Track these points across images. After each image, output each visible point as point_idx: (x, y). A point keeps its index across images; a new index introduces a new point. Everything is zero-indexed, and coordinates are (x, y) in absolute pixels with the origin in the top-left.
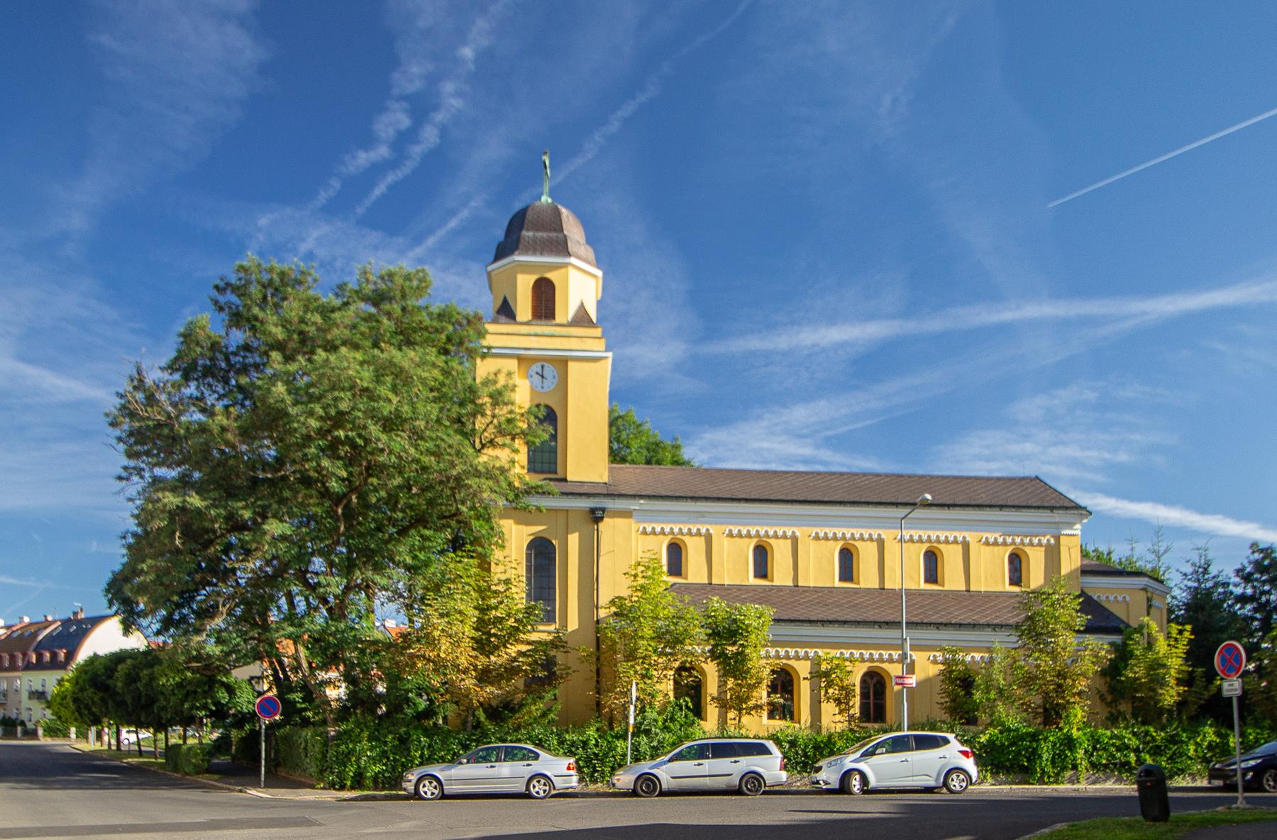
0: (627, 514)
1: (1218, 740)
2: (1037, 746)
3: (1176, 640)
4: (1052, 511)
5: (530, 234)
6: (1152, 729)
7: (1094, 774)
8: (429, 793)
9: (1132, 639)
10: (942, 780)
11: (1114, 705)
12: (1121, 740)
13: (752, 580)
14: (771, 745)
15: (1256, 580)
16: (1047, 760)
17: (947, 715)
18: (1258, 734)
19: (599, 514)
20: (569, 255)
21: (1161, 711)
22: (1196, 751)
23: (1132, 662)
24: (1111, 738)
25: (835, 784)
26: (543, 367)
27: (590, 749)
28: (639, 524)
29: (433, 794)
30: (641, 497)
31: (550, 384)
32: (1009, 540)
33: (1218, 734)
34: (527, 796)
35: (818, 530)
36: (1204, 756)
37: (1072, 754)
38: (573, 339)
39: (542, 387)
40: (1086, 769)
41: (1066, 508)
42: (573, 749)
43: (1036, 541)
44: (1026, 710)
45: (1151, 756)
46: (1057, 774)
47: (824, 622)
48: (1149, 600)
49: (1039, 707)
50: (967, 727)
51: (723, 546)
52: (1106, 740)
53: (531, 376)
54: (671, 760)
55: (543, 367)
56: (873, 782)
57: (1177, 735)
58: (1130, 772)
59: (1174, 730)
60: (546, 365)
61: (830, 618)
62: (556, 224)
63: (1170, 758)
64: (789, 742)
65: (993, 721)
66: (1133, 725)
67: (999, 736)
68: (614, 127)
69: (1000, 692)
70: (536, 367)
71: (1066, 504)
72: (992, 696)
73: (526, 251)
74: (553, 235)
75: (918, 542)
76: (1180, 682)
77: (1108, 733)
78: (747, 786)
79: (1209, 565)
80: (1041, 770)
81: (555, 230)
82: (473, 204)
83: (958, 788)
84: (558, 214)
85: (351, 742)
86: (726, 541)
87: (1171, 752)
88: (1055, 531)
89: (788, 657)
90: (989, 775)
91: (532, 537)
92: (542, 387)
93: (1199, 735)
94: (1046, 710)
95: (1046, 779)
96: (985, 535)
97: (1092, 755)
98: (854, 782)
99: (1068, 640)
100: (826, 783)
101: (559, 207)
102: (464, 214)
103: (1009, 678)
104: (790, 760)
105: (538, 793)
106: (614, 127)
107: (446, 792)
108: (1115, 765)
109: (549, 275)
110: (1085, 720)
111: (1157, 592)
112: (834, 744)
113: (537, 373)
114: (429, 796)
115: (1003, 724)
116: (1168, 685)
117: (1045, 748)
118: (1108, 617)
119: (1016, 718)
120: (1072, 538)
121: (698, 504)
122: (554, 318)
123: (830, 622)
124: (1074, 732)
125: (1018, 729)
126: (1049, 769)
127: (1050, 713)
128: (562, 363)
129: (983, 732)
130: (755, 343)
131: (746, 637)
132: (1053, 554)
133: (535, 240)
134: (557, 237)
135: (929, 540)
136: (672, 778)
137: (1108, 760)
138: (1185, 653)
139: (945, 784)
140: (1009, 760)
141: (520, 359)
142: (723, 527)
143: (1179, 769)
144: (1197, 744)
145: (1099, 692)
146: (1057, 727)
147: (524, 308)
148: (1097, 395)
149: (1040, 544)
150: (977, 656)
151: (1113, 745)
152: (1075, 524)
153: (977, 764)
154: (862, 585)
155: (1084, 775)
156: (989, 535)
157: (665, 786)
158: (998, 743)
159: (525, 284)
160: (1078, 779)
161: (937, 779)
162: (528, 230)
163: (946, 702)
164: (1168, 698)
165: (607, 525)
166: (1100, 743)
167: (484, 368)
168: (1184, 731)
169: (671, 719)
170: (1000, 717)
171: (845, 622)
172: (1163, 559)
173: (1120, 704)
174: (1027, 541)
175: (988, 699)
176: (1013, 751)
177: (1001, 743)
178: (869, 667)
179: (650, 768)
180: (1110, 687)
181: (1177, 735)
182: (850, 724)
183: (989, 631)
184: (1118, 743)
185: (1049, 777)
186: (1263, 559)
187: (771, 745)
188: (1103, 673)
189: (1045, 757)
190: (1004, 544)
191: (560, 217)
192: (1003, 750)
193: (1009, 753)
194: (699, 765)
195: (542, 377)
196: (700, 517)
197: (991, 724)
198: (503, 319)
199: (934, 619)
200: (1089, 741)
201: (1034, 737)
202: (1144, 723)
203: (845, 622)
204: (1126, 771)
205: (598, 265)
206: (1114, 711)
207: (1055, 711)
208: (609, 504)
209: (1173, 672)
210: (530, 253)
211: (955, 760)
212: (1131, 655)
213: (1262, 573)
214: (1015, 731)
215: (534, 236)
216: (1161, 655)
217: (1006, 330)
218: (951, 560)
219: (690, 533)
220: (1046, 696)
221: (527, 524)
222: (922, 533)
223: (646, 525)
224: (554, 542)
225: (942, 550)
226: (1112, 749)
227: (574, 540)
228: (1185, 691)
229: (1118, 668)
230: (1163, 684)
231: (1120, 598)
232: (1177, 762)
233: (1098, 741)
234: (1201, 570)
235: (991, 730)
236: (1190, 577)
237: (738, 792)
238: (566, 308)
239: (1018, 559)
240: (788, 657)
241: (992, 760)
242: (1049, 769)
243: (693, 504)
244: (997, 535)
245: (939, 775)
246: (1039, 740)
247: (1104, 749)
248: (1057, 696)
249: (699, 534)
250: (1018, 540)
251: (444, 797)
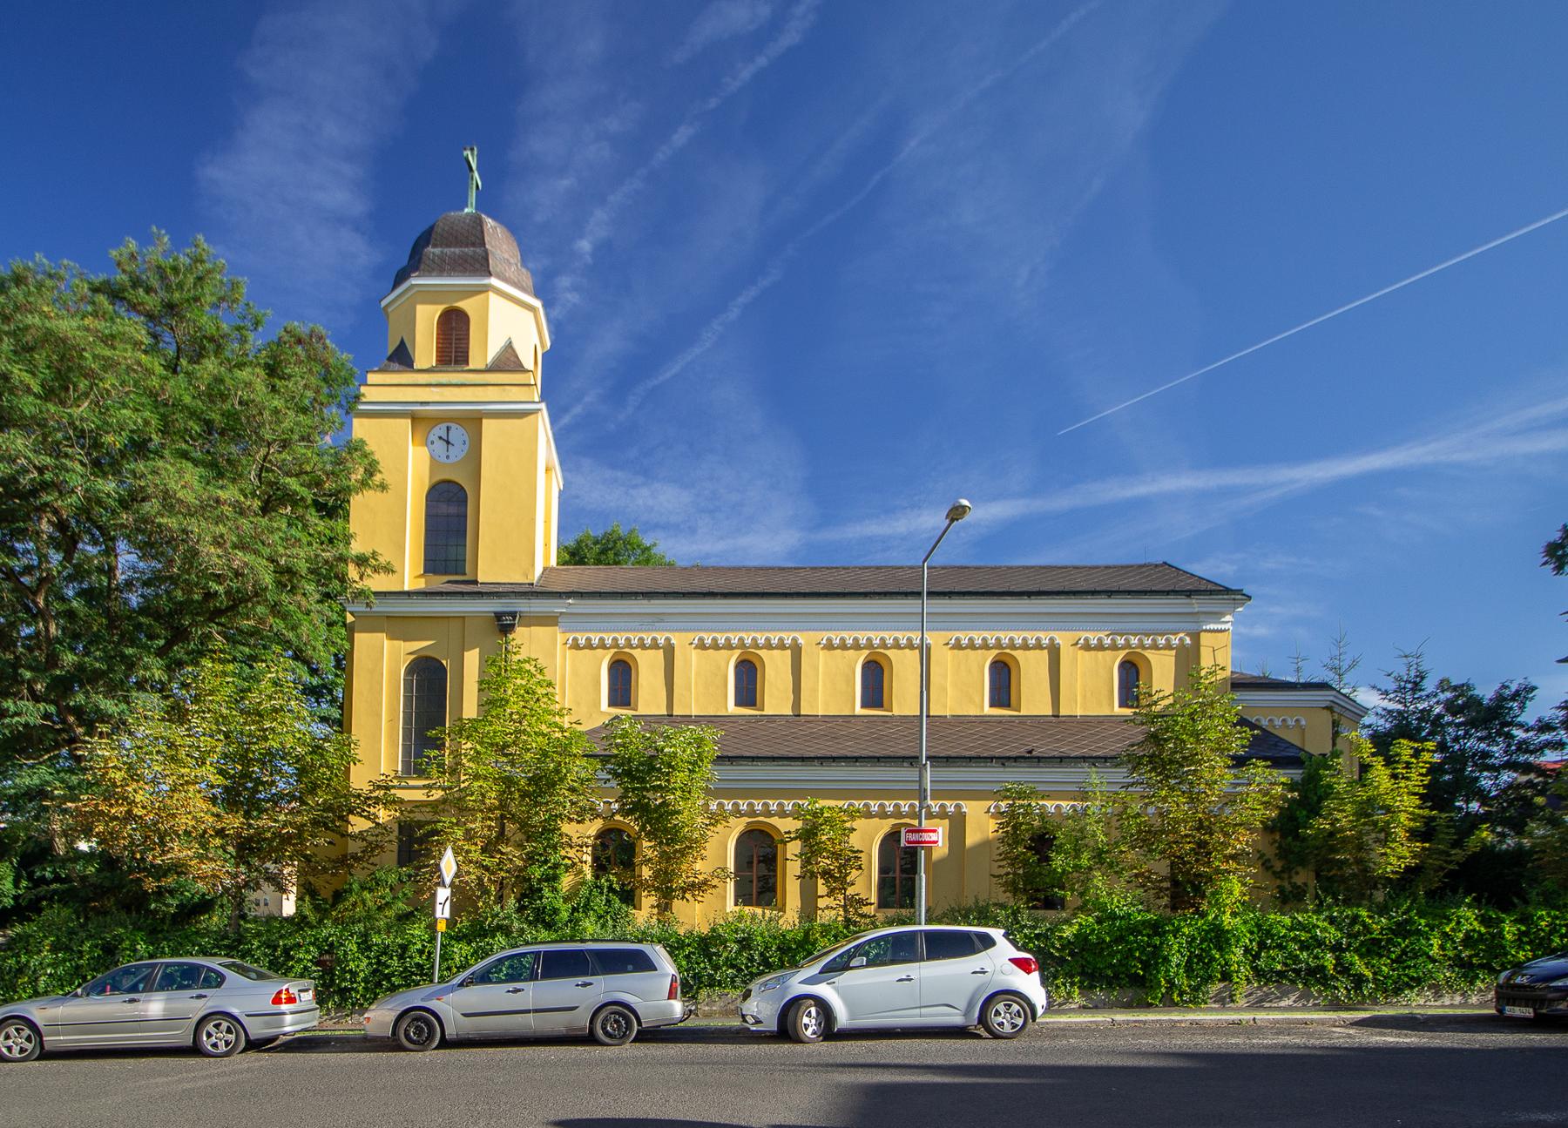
0: (549, 620)
1: (1483, 930)
2: (1161, 943)
3: (1408, 765)
4: (1189, 596)
5: (437, 251)
6: (1364, 913)
7: (1260, 988)
8: (16, 1049)
9: (1329, 768)
10: (976, 1014)
11: (1286, 876)
12: (1309, 932)
13: (732, 709)
14: (659, 954)
15: (1449, 724)
16: (1178, 965)
17: (1008, 894)
18: (1557, 918)
19: (507, 620)
20: (490, 274)
21: (1373, 883)
22: (1442, 947)
23: (1330, 803)
24: (1291, 929)
25: (772, 1025)
26: (448, 429)
27: (411, 957)
28: (568, 635)
29: (22, 1050)
30: (569, 594)
31: (458, 452)
32: (1121, 641)
33: (1484, 920)
34: (195, 1050)
35: (832, 635)
36: (1458, 956)
37: (1222, 956)
38: (490, 388)
39: (448, 457)
40: (1247, 979)
41: (1211, 592)
42: (384, 959)
43: (1161, 641)
44: (1142, 886)
45: (1361, 957)
46: (1196, 989)
47: (823, 760)
48: (1335, 724)
49: (1164, 879)
50: (1041, 913)
51: (691, 662)
52: (1284, 931)
53: (432, 443)
54: (461, 985)
55: (448, 429)
56: (843, 1019)
57: (1409, 921)
58: (1323, 985)
59: (1404, 914)
60: (453, 426)
61: (834, 755)
62: (474, 236)
63: (1398, 960)
64: (737, 941)
65: (1085, 903)
66: (1329, 907)
67: (1096, 927)
68: (734, 313)
69: (1099, 855)
70: (440, 430)
71: (1210, 587)
72: (1085, 861)
73: (429, 272)
74: (469, 250)
75: (981, 648)
76: (1414, 835)
77: (1287, 920)
78: (604, 1029)
79: (1423, 678)
80: (1168, 982)
81: (473, 245)
82: (587, 399)
83: (1007, 1029)
84: (479, 223)
85: (27, 952)
86: (695, 654)
87: (1398, 950)
88: (1192, 627)
89: (769, 814)
90: (1077, 991)
91: (413, 657)
92: (448, 457)
93: (1450, 921)
94: (1175, 883)
95: (1176, 998)
96: (1084, 635)
97: (1257, 957)
98: (806, 1020)
99: (1217, 774)
100: (758, 1022)
101: (483, 216)
102: (578, 410)
103: (1116, 834)
104: (739, 970)
105: (215, 1045)
106: (734, 313)
107: (47, 1047)
108: (1297, 972)
109: (462, 305)
110: (1246, 898)
111: (1347, 714)
112: (814, 944)
113: (440, 438)
114: (16, 1053)
115: (1103, 908)
116: (1394, 841)
117: (1176, 947)
118: (1276, 745)
119: (1125, 898)
120: (1220, 634)
121: (652, 602)
122: (468, 364)
123: (834, 759)
124: (1227, 919)
125: (1130, 915)
126: (1182, 981)
127: (1185, 889)
128: (473, 421)
129: (1067, 922)
130: (873, 528)
131: (668, 774)
132: (1188, 659)
133: (442, 258)
134: (475, 252)
135: (998, 645)
136: (465, 1015)
137: (1285, 964)
138: (1424, 786)
139: (983, 1020)
140: (1111, 966)
141: (415, 418)
142: (691, 636)
143: (1412, 979)
144: (1445, 935)
145: (1262, 856)
146: (1197, 912)
147: (425, 350)
148: (1235, 567)
149: (1168, 647)
150: (1065, 805)
151: (1295, 939)
152: (1224, 615)
153: (1044, 982)
154: (896, 712)
155: (1242, 989)
156: (1090, 635)
157: (451, 1032)
158: (1093, 938)
159: (427, 318)
160: (1231, 996)
161: (967, 1013)
162: (435, 246)
163: (1008, 874)
164: (1393, 860)
165: (520, 634)
166: (1271, 937)
167: (361, 428)
168: (1421, 914)
169: (586, 906)
170: (1098, 897)
171: (857, 759)
172: (1346, 678)
173: (1297, 873)
174: (1148, 641)
175: (1077, 868)
176: (1119, 951)
177: (1098, 938)
178: (894, 825)
179: (422, 1000)
180: (1280, 847)
181: (1409, 921)
182: (846, 911)
183: (1086, 767)
184: (1304, 936)
185: (1181, 994)
186: (1457, 697)
187: (659, 954)
188: (1269, 828)
189: (1175, 960)
190: (1114, 647)
191: (482, 227)
192: (1102, 949)
193: (1112, 955)
194: (516, 991)
195: (448, 442)
196: (658, 620)
197: (1082, 908)
198: (396, 366)
199: (998, 752)
200: (1252, 933)
201: (1156, 928)
202: (1347, 903)
203: (857, 759)
204: (1318, 981)
205: (537, 295)
206: (1286, 884)
207: (1193, 885)
208: (521, 606)
209: (1403, 817)
210: (435, 274)
211: (1004, 977)
212: (1328, 792)
213: (1454, 714)
214: (1122, 918)
215: (442, 252)
216: (1382, 790)
217: (1140, 506)
218: (1032, 671)
219: (642, 646)
220: (1177, 863)
221: (407, 638)
222: (987, 634)
223: (578, 635)
224: (444, 662)
225: (1019, 659)
226: (1293, 946)
227: (472, 659)
228: (1423, 849)
229: (1296, 819)
230: (1385, 835)
231: (1291, 722)
232: (1409, 967)
233: (1268, 934)
234: (1409, 686)
235: (1081, 918)
236: (1392, 696)
237: (589, 1039)
238: (486, 347)
239: (1133, 670)
240: (769, 814)
241: (1083, 966)
242: (1182, 981)
243: (646, 602)
244: (1102, 635)
245: (970, 1005)
246: (1165, 932)
247: (1280, 947)
248: (1197, 861)
249: (655, 645)
250: (1134, 641)
251: (46, 1055)
